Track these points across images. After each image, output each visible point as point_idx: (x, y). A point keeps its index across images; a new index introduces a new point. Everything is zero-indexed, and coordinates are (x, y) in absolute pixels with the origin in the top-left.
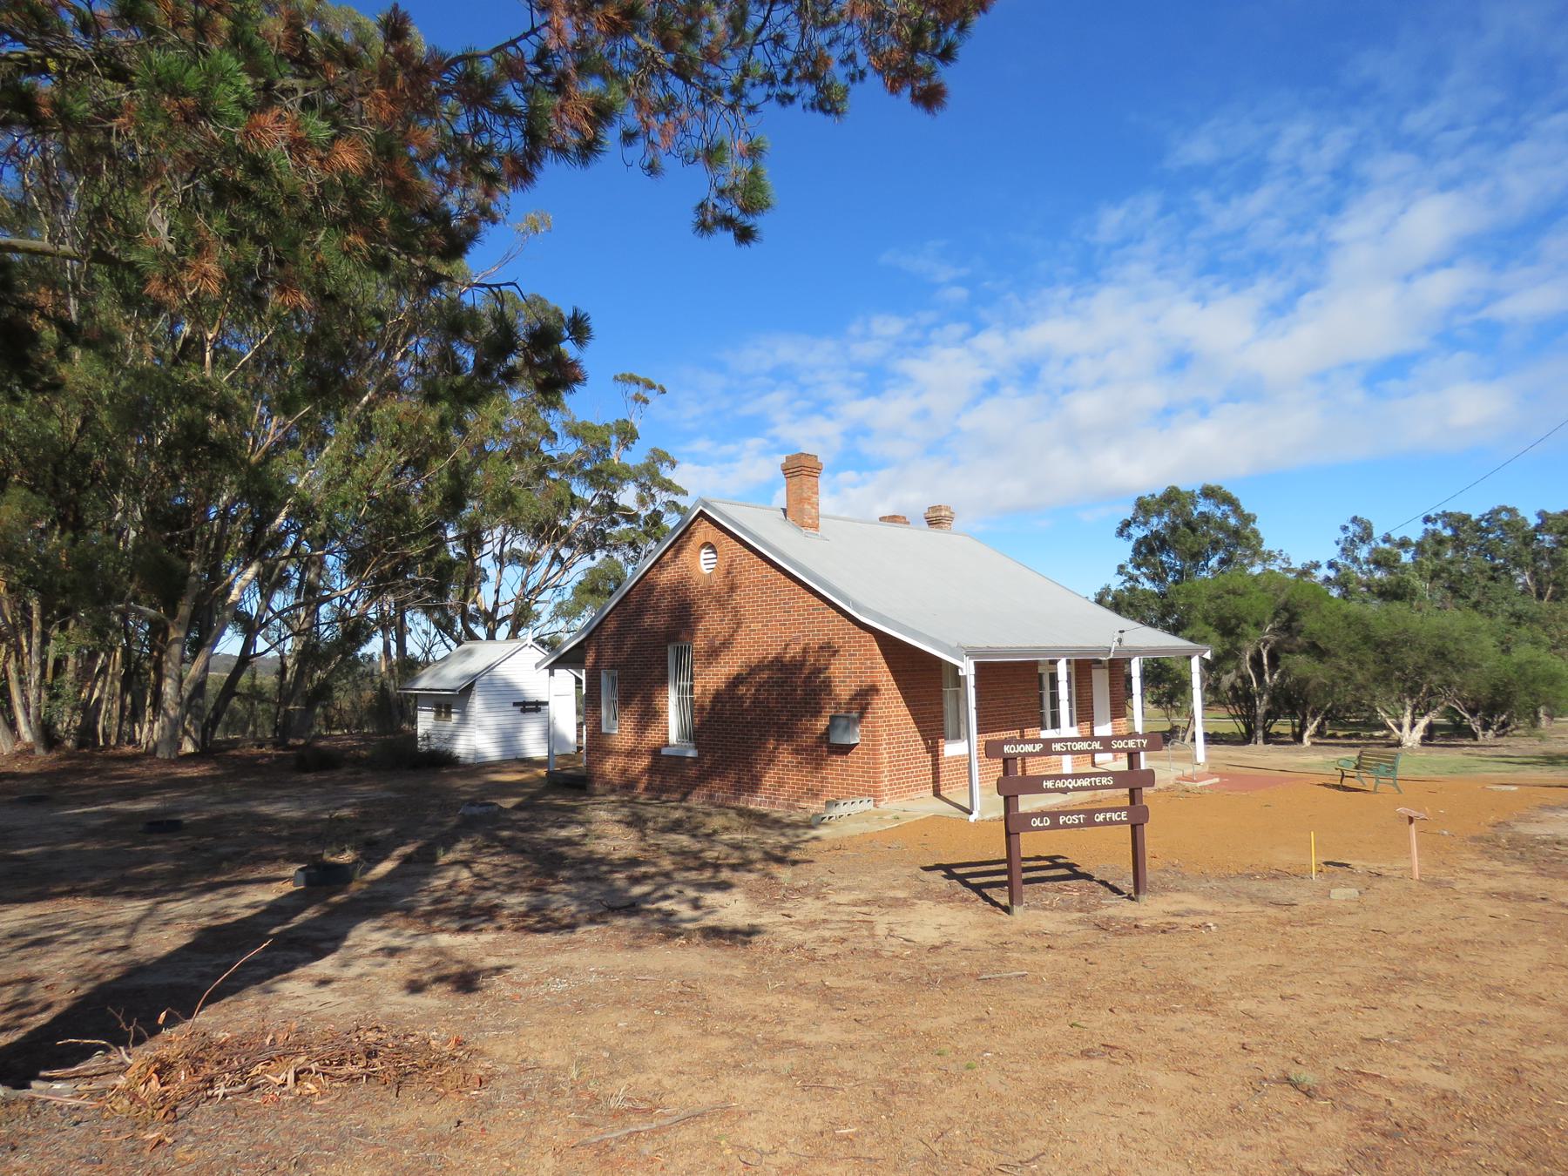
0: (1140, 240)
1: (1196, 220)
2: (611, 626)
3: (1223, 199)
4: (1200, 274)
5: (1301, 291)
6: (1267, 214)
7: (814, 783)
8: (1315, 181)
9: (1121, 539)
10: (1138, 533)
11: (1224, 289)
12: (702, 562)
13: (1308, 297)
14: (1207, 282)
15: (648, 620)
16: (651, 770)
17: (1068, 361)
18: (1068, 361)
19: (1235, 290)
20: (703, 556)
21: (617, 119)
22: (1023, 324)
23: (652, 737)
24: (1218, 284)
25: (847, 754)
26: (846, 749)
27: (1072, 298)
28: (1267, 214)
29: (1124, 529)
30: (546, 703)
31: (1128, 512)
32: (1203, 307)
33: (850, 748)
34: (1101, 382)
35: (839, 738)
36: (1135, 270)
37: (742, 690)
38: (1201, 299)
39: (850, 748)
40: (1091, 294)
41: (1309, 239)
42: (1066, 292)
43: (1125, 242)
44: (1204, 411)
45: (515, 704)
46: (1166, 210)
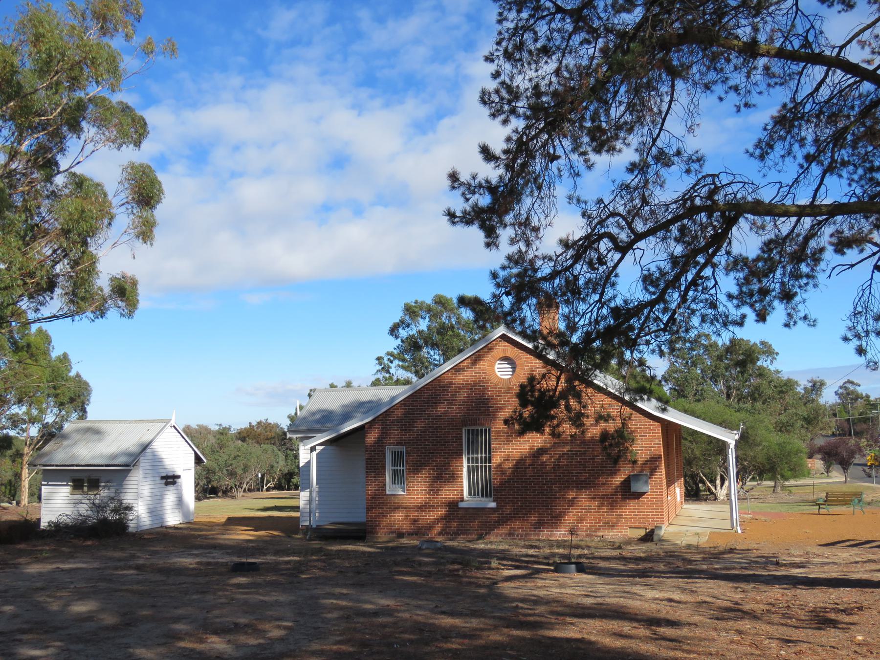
0: (309, 43)
1: (358, 35)
2: (399, 413)
3: (381, 20)
4: (360, 84)
5: (441, 114)
6: (416, 41)
7: (611, 517)
8: (455, 19)
9: (391, 337)
10: (403, 333)
11: (378, 102)
12: (497, 370)
13: (446, 122)
14: (364, 93)
15: (441, 409)
16: (447, 518)
17: (237, 148)
18: (237, 148)
19: (387, 105)
20: (497, 366)
21: (739, 196)
22: (194, 105)
23: (447, 493)
24: (372, 97)
25: (638, 498)
26: (639, 495)
27: (244, 88)
28: (416, 41)
29: (393, 331)
30: (179, 477)
31: (397, 315)
32: (359, 115)
33: (642, 494)
34: (267, 172)
35: (636, 487)
36: (302, 71)
37: (544, 458)
38: (359, 108)
39: (642, 494)
40: (262, 87)
41: (448, 70)
42: (236, 81)
43: (295, 42)
44: (358, 211)
45: (163, 478)
46: (331, 21)
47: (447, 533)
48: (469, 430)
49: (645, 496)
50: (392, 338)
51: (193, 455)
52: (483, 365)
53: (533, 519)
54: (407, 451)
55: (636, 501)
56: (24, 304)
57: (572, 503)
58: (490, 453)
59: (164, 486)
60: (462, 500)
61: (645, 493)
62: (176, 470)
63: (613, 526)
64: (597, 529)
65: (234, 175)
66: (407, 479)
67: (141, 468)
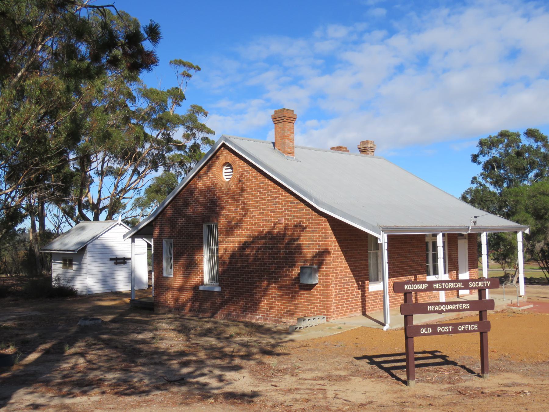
10: (483, 159)
11: (541, 10)
12: (224, 174)
15: (191, 210)
16: (193, 299)
17: (446, 54)
20: (224, 171)
22: (419, 31)
24: (537, 7)
25: (310, 289)
26: (310, 287)
27: (449, 15)
32: (528, 21)
37: (248, 251)
38: (527, 16)
40: (461, 13)
42: (445, 11)
44: (527, 83)
47: (194, 310)
48: (209, 226)
49: (315, 288)
50: (475, 165)
51: (146, 244)
52: (214, 170)
53: (242, 303)
54: (173, 243)
55: (309, 292)
56: (139, 150)
57: (265, 292)
58: (217, 245)
59: (114, 265)
60: (202, 284)
61: (316, 284)
62: (126, 254)
63: (293, 314)
64: (282, 315)
65: (445, 71)
66: (174, 265)
67: (88, 253)
